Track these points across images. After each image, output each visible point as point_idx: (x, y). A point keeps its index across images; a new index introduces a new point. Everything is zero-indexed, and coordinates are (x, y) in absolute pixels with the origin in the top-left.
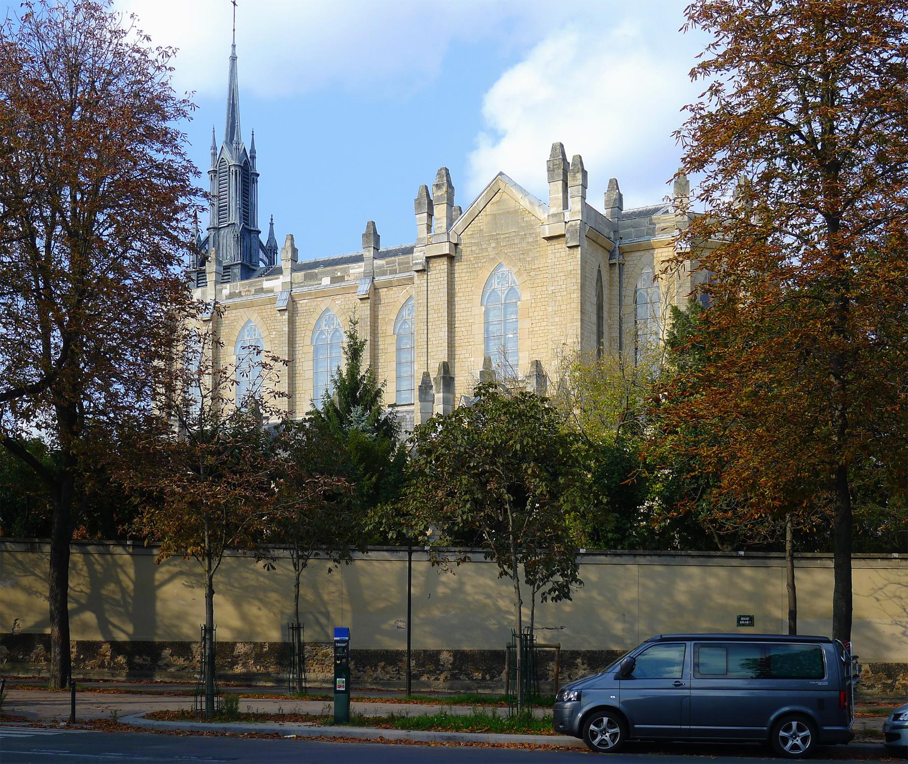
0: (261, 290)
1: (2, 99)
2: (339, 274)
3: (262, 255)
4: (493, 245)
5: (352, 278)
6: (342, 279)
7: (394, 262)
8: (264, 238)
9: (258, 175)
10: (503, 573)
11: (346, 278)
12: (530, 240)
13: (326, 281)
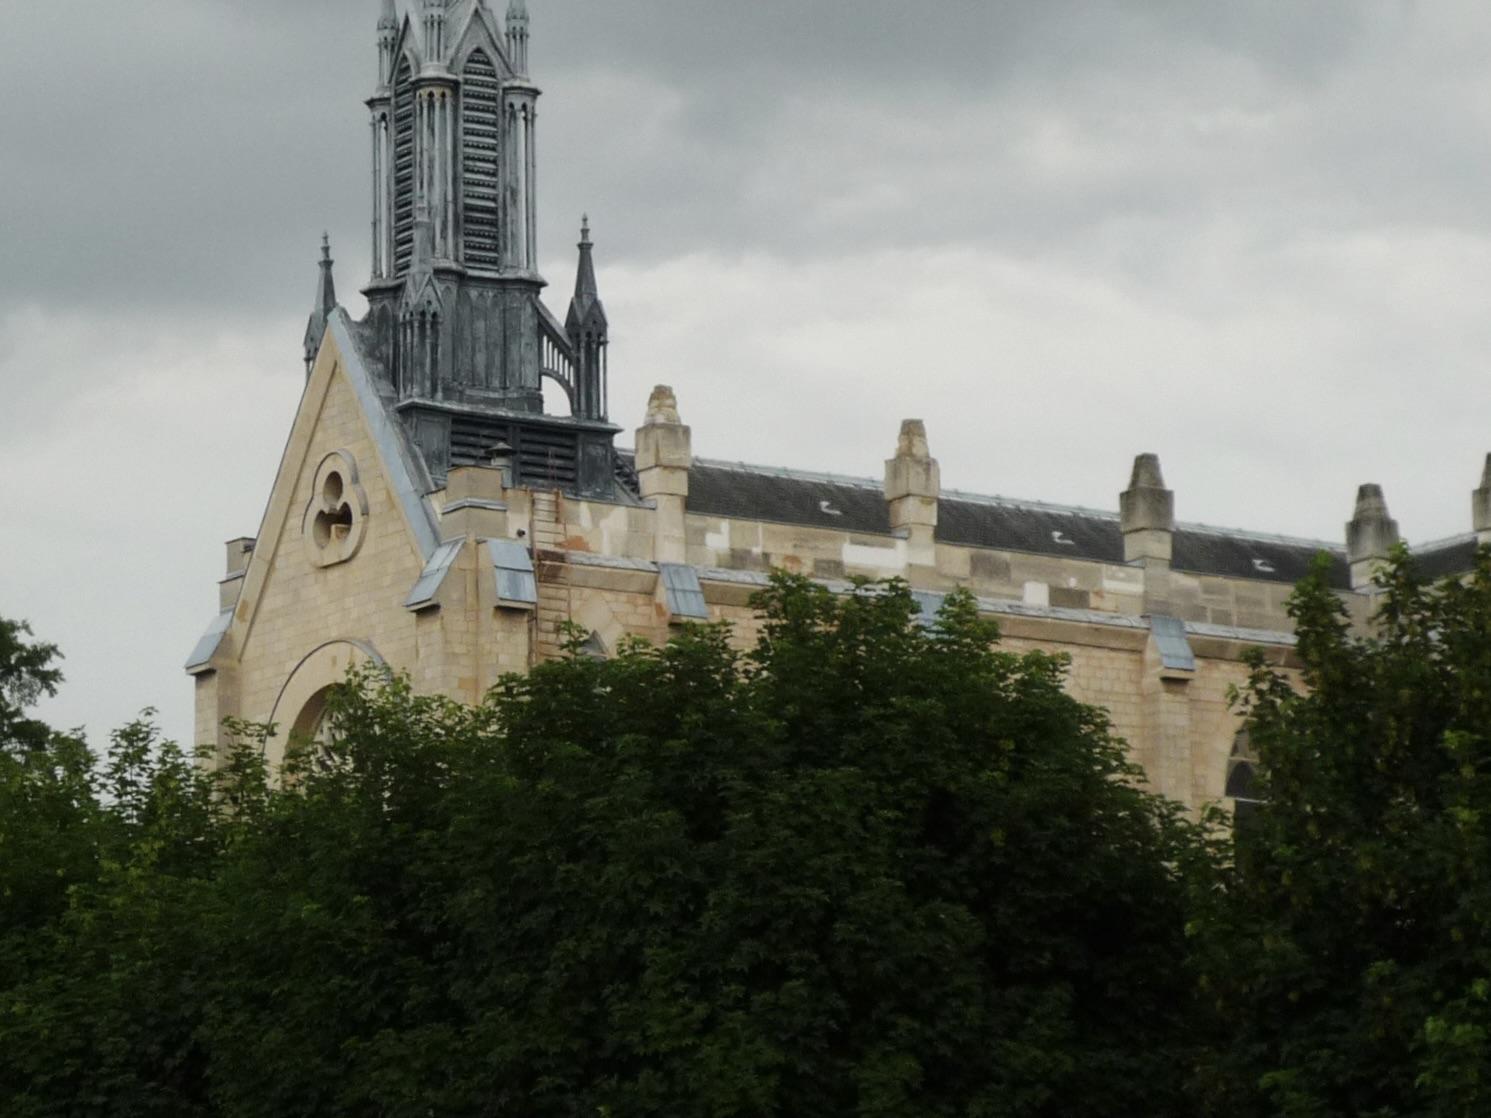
3: (551, 357)
8: (557, 301)
11: (1094, 601)
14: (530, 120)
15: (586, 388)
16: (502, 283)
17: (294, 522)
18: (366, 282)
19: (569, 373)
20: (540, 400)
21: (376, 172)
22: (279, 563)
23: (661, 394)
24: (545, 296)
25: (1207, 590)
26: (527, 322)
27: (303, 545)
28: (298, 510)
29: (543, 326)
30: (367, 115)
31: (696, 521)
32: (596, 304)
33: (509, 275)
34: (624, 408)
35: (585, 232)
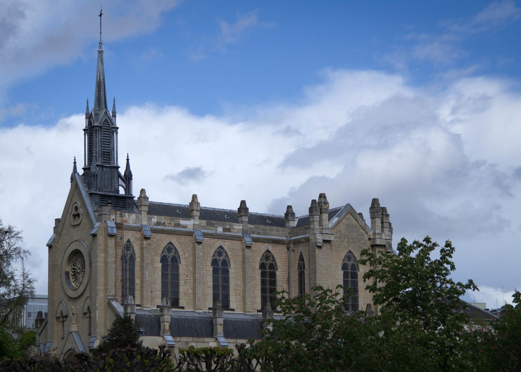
0: (178, 225)
1: (2, 292)
2: (228, 227)
3: (121, 182)
4: (346, 240)
5: (235, 231)
6: (229, 230)
7: (259, 228)
8: (122, 171)
9: (118, 128)
10: (30, 282)
11: (232, 230)
12: (363, 242)
13: (220, 230)
14: (117, 133)
15: (128, 189)
16: (111, 167)
17: (68, 216)
18: (83, 166)
19: (124, 185)
20: (119, 191)
21: (117, 153)
22: (65, 224)
23: (143, 191)
24: (120, 170)
25: (255, 228)
26: (116, 175)
27: (71, 220)
28: (69, 213)
29: (119, 175)
30: (83, 131)
31: (150, 216)
32: (130, 171)
33: (112, 165)
34: (136, 193)
35: (128, 157)
